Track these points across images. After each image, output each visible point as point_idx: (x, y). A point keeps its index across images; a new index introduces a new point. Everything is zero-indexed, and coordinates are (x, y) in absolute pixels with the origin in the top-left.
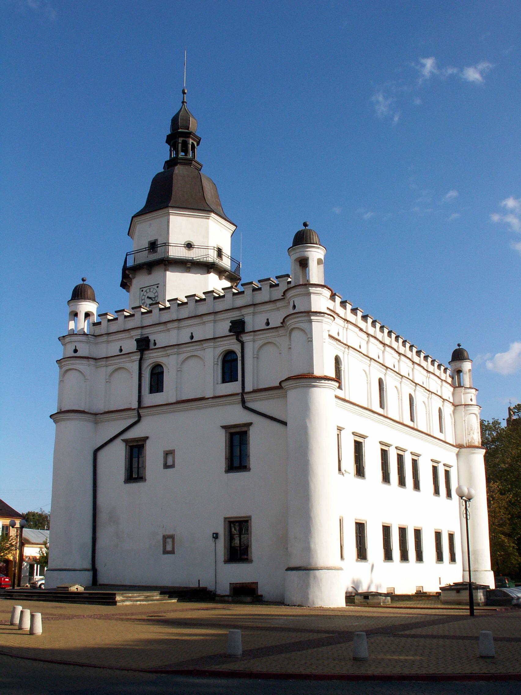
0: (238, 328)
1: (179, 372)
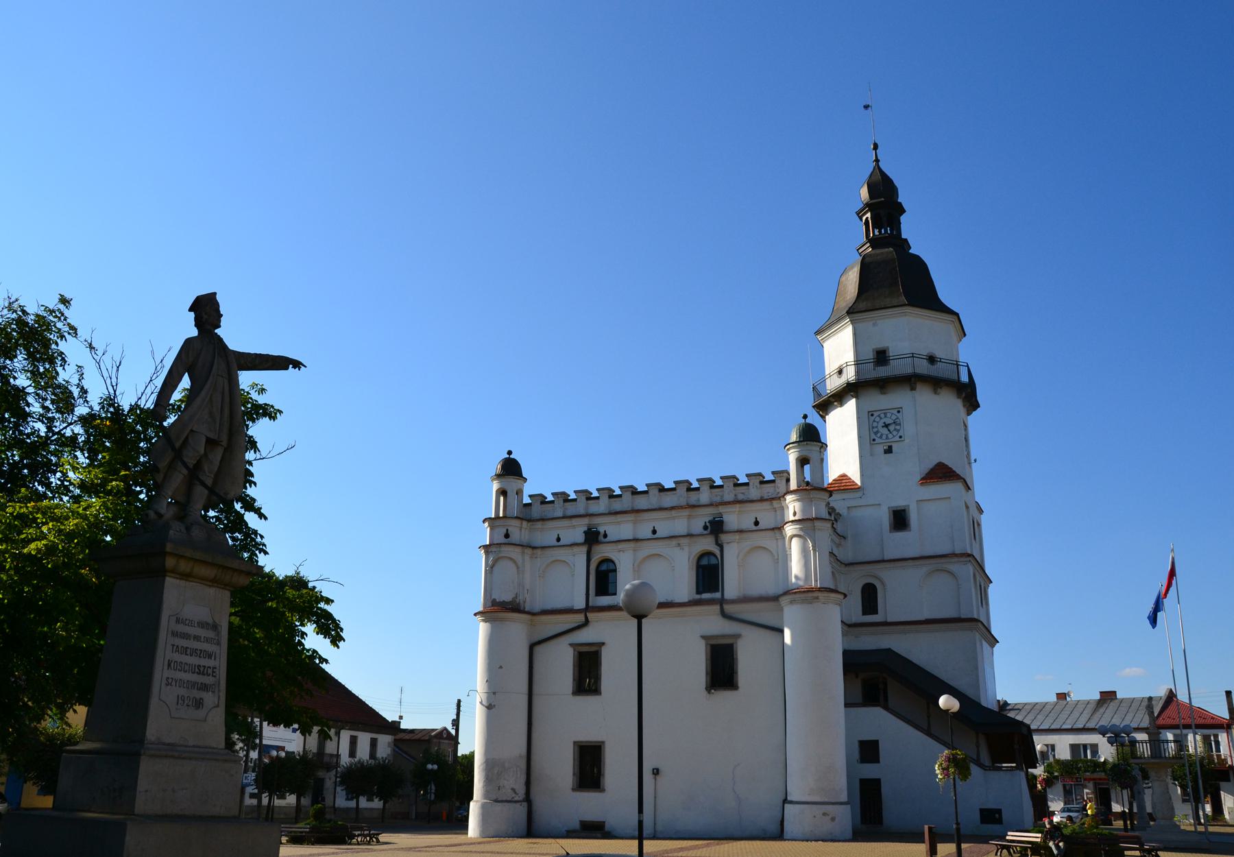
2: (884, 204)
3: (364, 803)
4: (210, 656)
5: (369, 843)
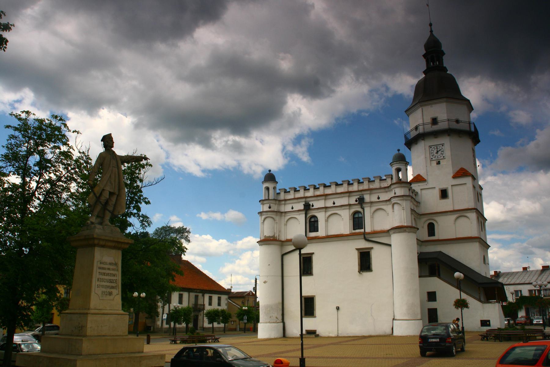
0: (361, 201)
3: (216, 325)
4: (114, 276)
5: (214, 342)
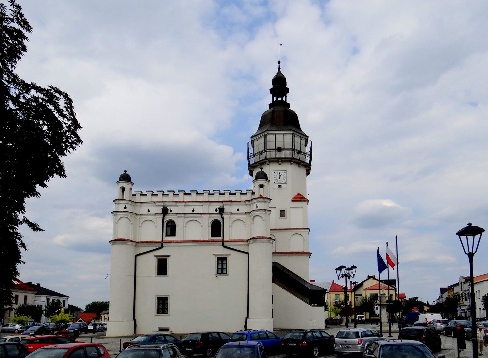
1: (140, 227)
2: (279, 86)
